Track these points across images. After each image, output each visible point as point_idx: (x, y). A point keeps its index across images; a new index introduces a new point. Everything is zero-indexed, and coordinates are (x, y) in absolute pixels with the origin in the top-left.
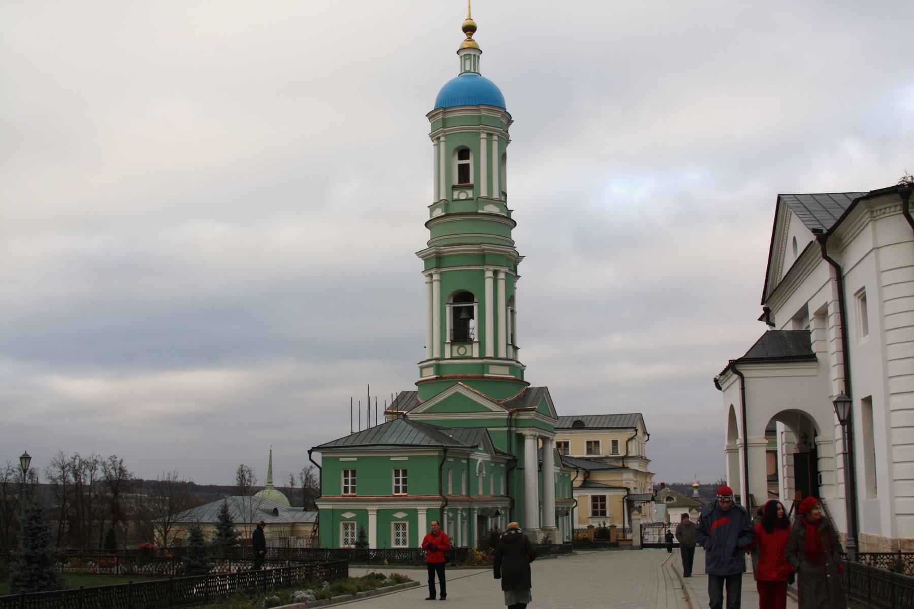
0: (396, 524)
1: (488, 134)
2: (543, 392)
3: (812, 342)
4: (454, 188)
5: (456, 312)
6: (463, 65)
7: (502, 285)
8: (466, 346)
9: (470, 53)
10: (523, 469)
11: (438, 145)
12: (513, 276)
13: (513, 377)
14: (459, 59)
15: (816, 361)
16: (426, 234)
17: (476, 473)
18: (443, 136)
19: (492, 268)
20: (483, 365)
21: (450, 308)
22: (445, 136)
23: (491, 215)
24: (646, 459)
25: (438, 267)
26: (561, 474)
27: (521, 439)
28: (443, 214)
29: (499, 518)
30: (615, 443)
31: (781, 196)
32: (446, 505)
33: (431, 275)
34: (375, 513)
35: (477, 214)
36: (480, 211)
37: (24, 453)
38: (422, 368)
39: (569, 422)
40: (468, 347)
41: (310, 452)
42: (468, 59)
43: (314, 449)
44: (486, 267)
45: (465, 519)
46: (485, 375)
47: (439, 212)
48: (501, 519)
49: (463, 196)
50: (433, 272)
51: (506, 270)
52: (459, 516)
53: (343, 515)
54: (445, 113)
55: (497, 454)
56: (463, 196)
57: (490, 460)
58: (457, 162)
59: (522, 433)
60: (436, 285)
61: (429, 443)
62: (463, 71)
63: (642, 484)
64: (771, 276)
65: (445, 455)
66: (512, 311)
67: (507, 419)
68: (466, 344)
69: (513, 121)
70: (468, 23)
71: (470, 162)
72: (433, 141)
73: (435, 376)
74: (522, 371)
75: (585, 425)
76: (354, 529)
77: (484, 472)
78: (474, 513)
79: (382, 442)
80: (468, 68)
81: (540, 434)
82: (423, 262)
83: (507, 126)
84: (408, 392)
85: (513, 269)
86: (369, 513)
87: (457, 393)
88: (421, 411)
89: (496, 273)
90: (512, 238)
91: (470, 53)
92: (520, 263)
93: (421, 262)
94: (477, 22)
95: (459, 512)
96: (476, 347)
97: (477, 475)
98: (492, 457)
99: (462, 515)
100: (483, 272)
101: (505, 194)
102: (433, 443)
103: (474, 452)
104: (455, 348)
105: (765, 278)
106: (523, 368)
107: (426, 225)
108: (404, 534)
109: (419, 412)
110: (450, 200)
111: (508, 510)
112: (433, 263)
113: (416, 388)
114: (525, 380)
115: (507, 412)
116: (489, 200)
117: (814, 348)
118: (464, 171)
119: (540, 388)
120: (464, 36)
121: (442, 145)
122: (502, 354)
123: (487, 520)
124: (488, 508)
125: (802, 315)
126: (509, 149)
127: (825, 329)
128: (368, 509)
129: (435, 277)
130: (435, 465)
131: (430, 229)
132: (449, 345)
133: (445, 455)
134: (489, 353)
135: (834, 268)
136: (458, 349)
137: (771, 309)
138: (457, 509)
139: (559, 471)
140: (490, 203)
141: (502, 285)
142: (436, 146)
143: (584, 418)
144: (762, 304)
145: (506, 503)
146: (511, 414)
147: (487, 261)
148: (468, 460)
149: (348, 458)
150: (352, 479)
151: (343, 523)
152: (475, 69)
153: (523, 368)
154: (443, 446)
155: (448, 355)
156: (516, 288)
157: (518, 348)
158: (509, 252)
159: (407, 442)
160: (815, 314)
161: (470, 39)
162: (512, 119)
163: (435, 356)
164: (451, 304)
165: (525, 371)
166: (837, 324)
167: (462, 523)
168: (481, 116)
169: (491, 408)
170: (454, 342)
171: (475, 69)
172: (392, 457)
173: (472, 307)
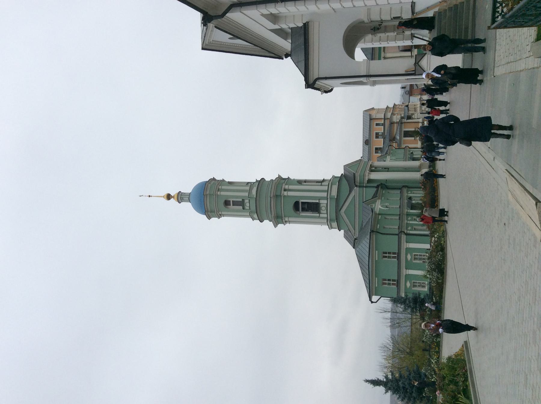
0: (414, 259)
1: (218, 191)
2: (346, 167)
3: (296, 26)
4: (243, 209)
5: (304, 210)
6: (185, 201)
7: (291, 187)
8: (321, 206)
9: (181, 197)
10: (386, 180)
11: (224, 215)
12: (288, 181)
13: (338, 183)
14: (183, 202)
15: (308, 22)
16: (266, 222)
17: (387, 209)
18: (219, 213)
19: (283, 192)
20: (330, 198)
21: (302, 213)
22: (219, 211)
23: (257, 191)
24: (386, 108)
25: (282, 218)
26: (391, 155)
27: (370, 181)
28: (256, 214)
29: (414, 153)
30: (377, 125)
31: (400, 50)
32: (404, 232)
33: (286, 222)
34: (407, 270)
35: (256, 198)
36: (255, 197)
37: (187, 206)
38: (332, 228)
39: (366, 147)
40: (321, 205)
41: (372, 302)
42: (183, 198)
43: (370, 300)
44: (282, 195)
45: (413, 218)
46: (336, 198)
47: (255, 216)
48: (414, 152)
49: (248, 205)
50: (284, 221)
51: (284, 184)
52: (411, 222)
53: (409, 260)
54: (208, 211)
55: (377, 196)
56: (248, 205)
57: (380, 200)
58: (231, 207)
59: (367, 180)
60: (290, 219)
61: (368, 239)
62: (189, 201)
63: (399, 110)
64: (249, 52)
65: (376, 232)
66: (305, 181)
67: (359, 188)
68: (320, 206)
69: (213, 177)
70: (165, 197)
71: (231, 200)
72: (221, 217)
73: (336, 222)
74: (336, 177)
75: (367, 139)
76: (417, 255)
77: (387, 204)
78: (409, 212)
79: (367, 263)
80: (187, 199)
81: (368, 170)
82: (279, 224)
83: (216, 181)
84: (344, 234)
85: (284, 181)
86: (407, 273)
87: (344, 212)
88: (354, 231)
89: (285, 190)
90: (270, 180)
91: (181, 197)
92: (282, 177)
93: (280, 226)
94: (165, 193)
95: (408, 195)
96: (321, 201)
97: (388, 209)
98: (379, 199)
99: (410, 220)
100: (284, 196)
101: (248, 183)
102: (368, 237)
103: (375, 211)
104: (322, 212)
105: (269, 58)
106: (334, 177)
107: (261, 222)
108: (421, 255)
109: (354, 228)
110: (250, 210)
111: (408, 189)
112: (280, 220)
113: (342, 231)
114: (340, 176)
115: (355, 188)
116: (250, 191)
117: (300, 25)
118: (235, 203)
119: (344, 169)
120: (172, 199)
121: (223, 213)
122: (326, 188)
123: (413, 203)
124: (407, 202)
125: (280, 32)
126: (227, 180)
127: (285, 16)
128: (405, 274)
129: (287, 219)
130: (380, 236)
131: (263, 221)
132: (320, 214)
133: (376, 232)
134: (325, 195)
135: (233, 8)
136: (322, 210)
137: (285, 53)
138: (407, 223)
139: (389, 156)
140: (251, 191)
141: (291, 187)
142: (224, 216)
143: (364, 139)
144: (283, 59)
145: (405, 190)
146: (356, 186)
147: (279, 194)
148: (379, 214)
149: (376, 282)
150: (386, 283)
151: (413, 287)
152: (187, 195)
153: (334, 177)
154: (370, 232)
155: (326, 216)
156: (294, 179)
157: (324, 179)
158: (275, 183)
159: (368, 250)
160: (275, 24)
161: (173, 197)
162: (213, 178)
163: (326, 222)
164: (300, 213)
165: (335, 176)
166: (274, 6)
167: (414, 193)
168: (209, 194)
169: (353, 196)
170: (319, 213)
171: (187, 195)
172: (376, 259)
173: (302, 202)
